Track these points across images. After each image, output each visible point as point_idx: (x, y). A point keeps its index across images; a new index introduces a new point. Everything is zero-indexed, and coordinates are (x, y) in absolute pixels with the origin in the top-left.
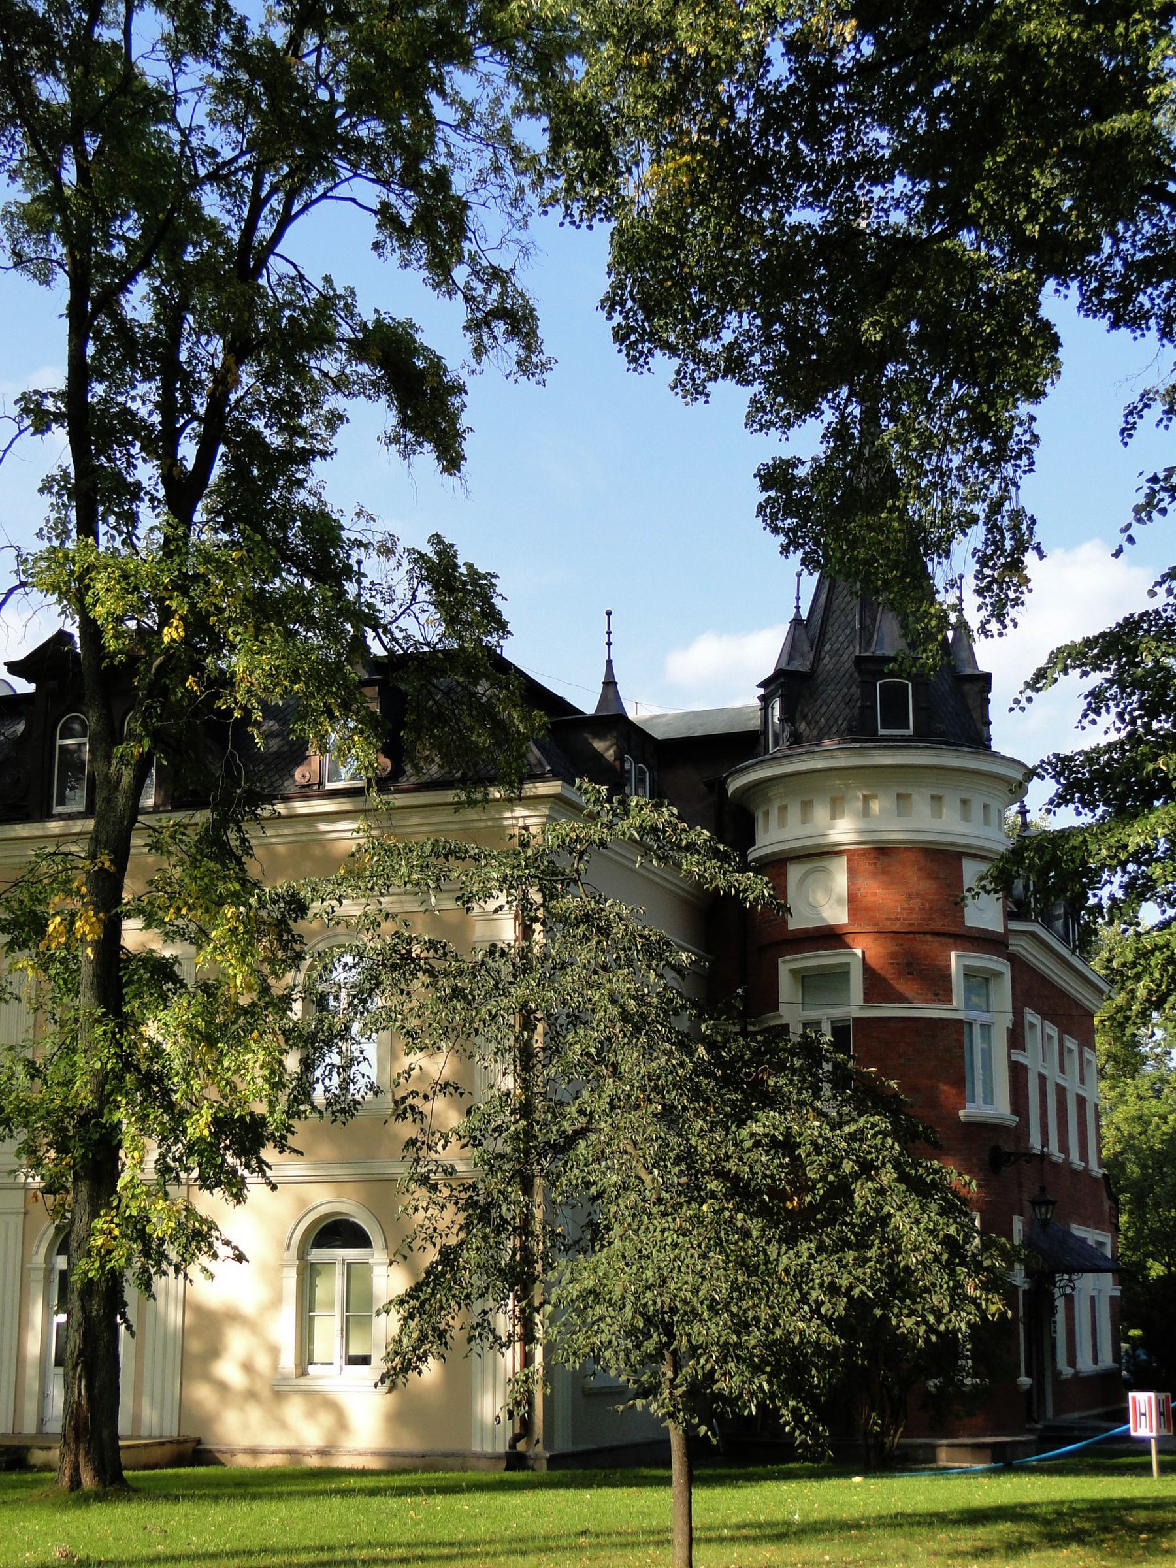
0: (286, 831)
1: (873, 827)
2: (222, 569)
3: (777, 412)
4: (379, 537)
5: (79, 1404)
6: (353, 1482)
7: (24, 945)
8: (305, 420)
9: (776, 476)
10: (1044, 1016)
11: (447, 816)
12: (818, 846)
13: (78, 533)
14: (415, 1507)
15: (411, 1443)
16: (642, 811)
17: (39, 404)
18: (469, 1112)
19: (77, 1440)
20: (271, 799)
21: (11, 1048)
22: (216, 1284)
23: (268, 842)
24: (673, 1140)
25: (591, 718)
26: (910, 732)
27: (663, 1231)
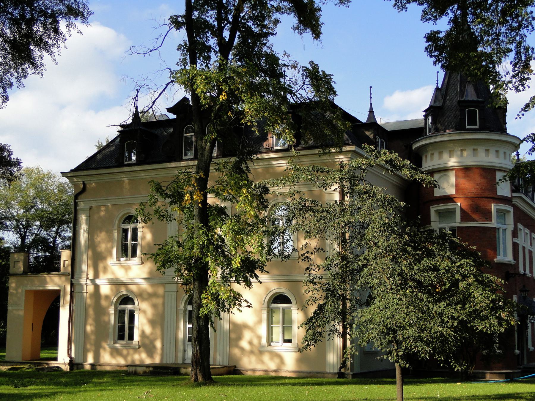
0: (261, 164)
1: (464, 161)
2: (239, 74)
3: (432, 14)
4: (292, 62)
5: (197, 354)
6: (287, 381)
7: (175, 203)
8: (266, 23)
9: (432, 37)
10: (525, 226)
11: (315, 159)
12: (445, 167)
13: (190, 63)
14: (308, 390)
15: (305, 368)
16: (386, 155)
17: (177, 19)
18: (326, 259)
19: (196, 366)
20: (256, 153)
21: (172, 237)
22: (240, 315)
23: (256, 167)
24: (397, 268)
25: (365, 124)
26: (478, 127)
27: (393, 299)
